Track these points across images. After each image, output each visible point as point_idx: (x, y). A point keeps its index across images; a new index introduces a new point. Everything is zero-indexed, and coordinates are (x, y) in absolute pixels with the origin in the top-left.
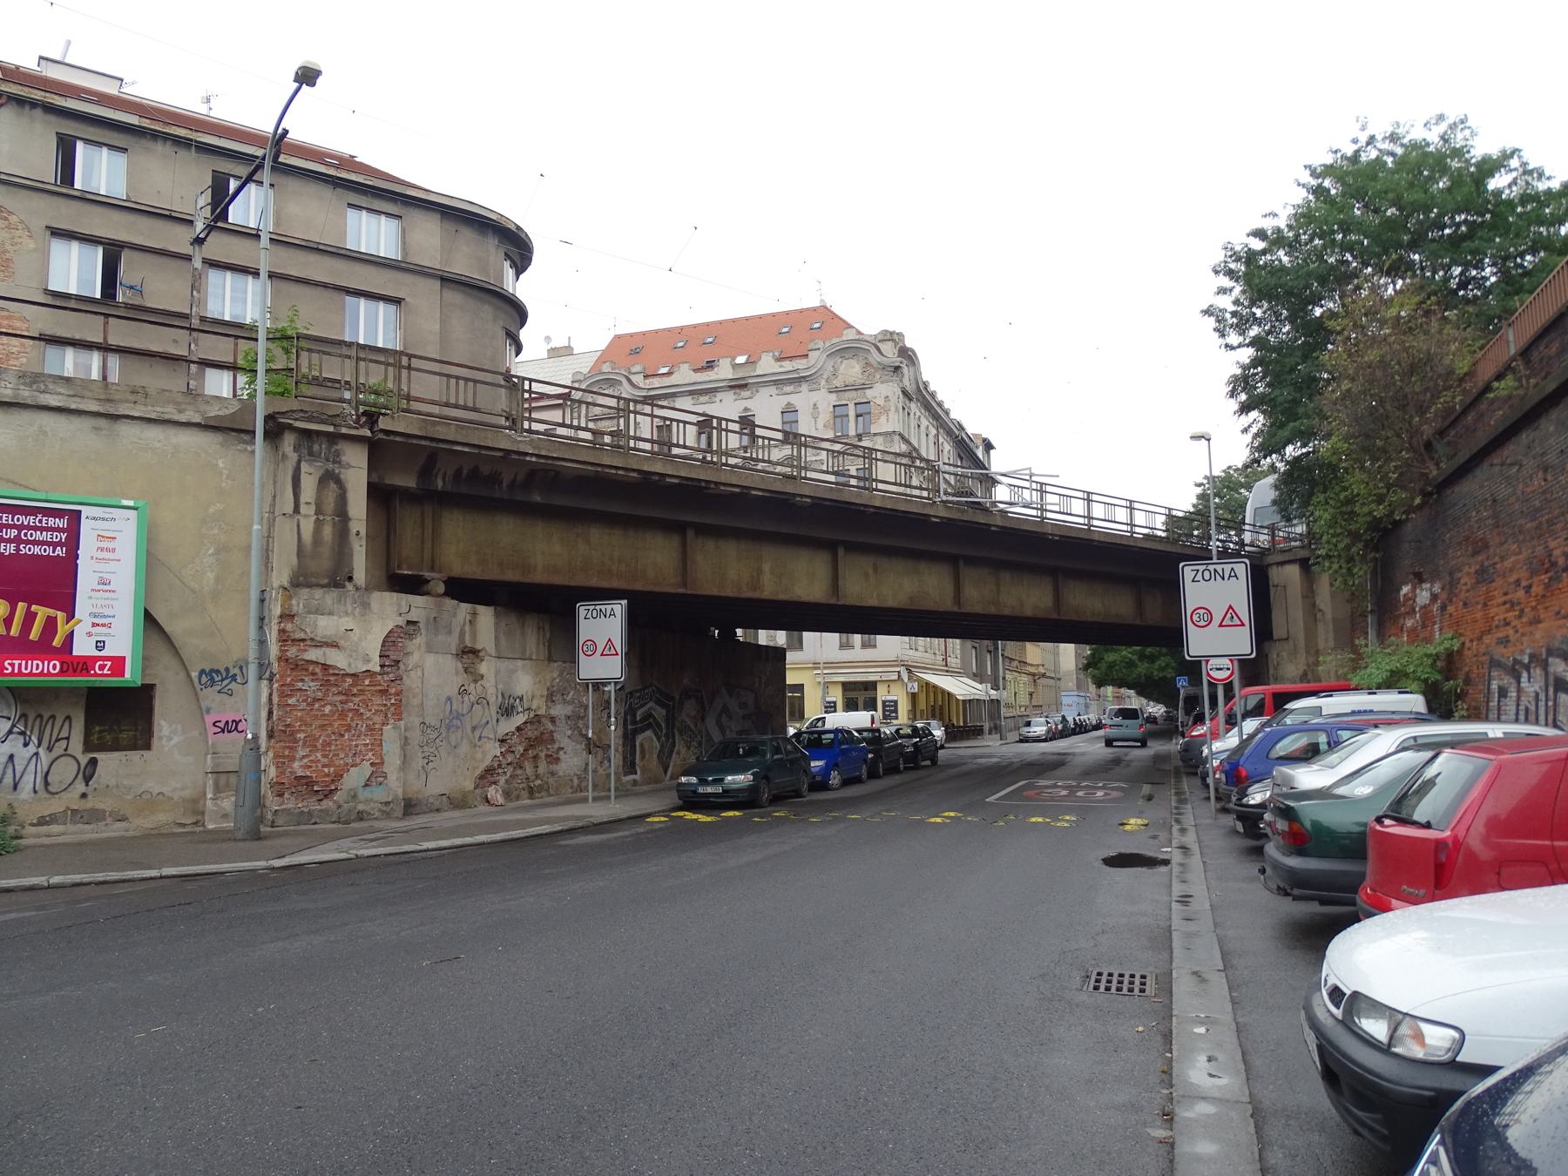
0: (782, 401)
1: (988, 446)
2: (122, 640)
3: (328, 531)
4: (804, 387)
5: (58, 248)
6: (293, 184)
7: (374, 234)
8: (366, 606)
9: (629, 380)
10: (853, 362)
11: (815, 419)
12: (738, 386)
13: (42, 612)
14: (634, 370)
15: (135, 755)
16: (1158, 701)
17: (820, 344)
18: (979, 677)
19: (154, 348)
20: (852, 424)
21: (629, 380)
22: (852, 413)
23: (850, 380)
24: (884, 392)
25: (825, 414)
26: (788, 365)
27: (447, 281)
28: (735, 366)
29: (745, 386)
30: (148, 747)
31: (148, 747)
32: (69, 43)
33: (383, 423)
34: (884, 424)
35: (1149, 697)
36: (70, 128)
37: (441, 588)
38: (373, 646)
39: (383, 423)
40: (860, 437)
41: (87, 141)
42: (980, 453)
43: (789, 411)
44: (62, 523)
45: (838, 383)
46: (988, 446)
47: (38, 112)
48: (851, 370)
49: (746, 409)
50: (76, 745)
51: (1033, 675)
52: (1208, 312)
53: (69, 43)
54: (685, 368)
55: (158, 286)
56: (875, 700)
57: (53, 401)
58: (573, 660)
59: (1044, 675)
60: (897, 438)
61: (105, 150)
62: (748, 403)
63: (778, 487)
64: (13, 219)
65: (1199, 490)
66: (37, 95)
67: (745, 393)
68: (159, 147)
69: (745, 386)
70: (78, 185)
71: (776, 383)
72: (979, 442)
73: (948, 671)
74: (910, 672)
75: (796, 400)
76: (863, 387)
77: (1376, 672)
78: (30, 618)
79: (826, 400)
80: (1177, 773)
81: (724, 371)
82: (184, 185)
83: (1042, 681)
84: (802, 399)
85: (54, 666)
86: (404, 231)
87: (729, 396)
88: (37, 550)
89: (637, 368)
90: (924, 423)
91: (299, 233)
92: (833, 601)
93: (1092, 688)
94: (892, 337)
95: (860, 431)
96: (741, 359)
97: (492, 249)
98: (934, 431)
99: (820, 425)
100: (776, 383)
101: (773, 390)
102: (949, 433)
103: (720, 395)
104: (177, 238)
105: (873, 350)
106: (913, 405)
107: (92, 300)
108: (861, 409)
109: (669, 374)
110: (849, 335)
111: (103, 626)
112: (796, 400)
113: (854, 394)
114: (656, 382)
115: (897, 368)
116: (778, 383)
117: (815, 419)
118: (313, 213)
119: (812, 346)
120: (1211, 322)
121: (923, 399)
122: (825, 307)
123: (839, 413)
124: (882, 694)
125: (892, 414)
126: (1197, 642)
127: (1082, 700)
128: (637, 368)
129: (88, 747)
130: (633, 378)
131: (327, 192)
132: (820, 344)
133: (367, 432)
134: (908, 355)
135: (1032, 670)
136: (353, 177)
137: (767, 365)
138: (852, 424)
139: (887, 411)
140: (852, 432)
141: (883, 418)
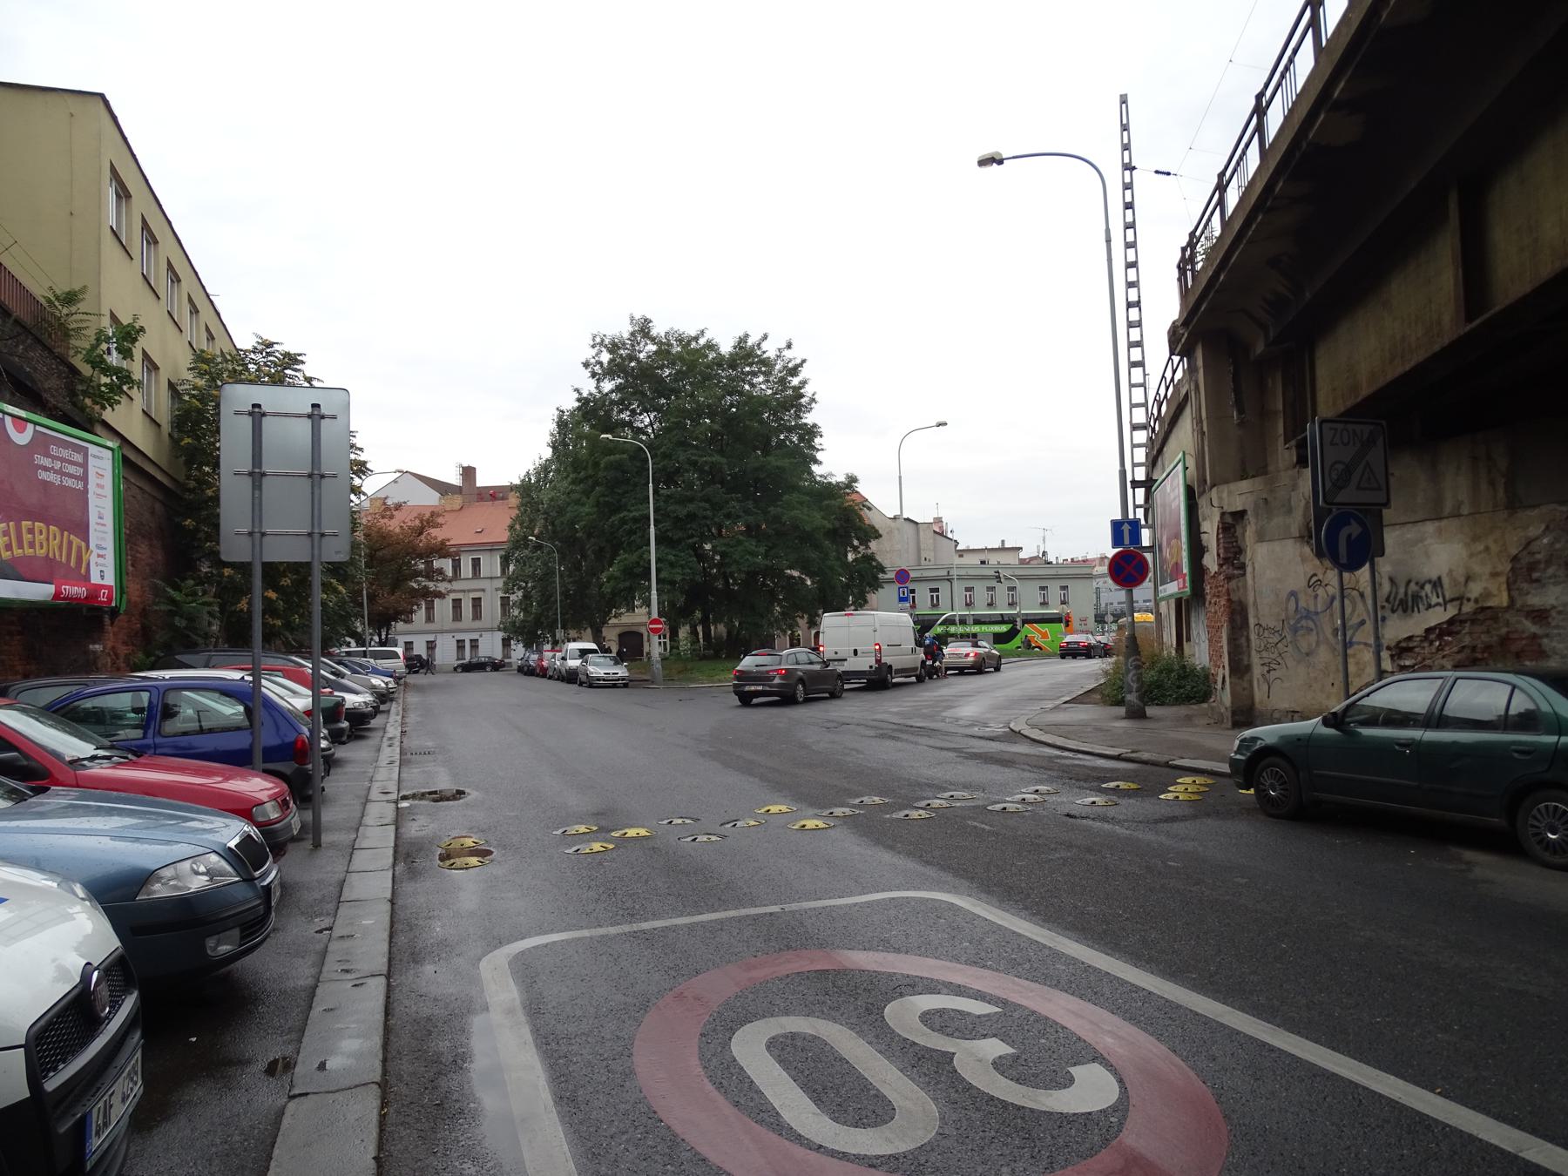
13: (76, 541)
44: (78, 458)
53: (1124, 100)
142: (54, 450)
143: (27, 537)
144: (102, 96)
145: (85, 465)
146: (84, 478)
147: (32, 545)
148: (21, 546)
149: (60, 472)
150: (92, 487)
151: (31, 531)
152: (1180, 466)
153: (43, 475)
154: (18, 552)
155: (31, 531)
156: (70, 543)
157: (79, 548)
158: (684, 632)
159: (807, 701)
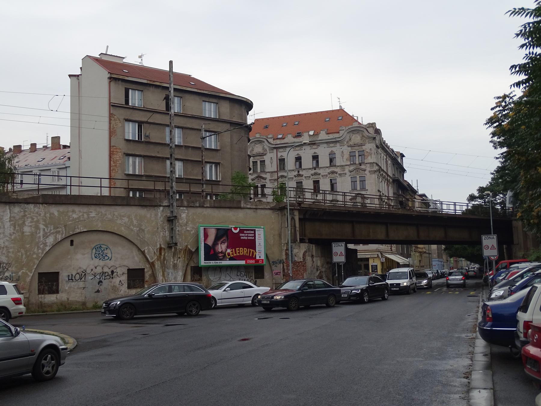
0: (329, 150)
1: (402, 156)
2: (263, 257)
3: (293, 230)
4: (338, 145)
5: (126, 124)
6: (187, 96)
7: (209, 110)
8: (300, 246)
9: (267, 141)
10: (357, 135)
11: (343, 157)
12: (312, 144)
13: (252, 250)
14: (269, 137)
15: (262, 280)
16: (475, 262)
17: (344, 128)
18: (402, 255)
19: (153, 155)
20: (357, 159)
21: (267, 141)
22: (357, 155)
23: (356, 142)
24: (369, 147)
25: (346, 156)
26: (331, 136)
27: (232, 123)
28: (310, 136)
29: (315, 144)
30: (263, 278)
31: (263, 278)
32: (108, 47)
33: (302, 205)
34: (369, 160)
35: (471, 261)
36: (128, 86)
37: (307, 241)
38: (301, 256)
39: (302, 205)
40: (360, 164)
41: (132, 89)
42: (399, 160)
43: (332, 154)
44: (253, 232)
45: (351, 143)
46: (402, 156)
47: (120, 82)
48: (356, 139)
49: (315, 153)
50: (253, 278)
51: (420, 252)
52: (491, 142)
53: (108, 47)
54: (290, 136)
55: (155, 135)
56: (368, 265)
57: (249, 206)
58: (331, 258)
59: (425, 252)
60: (375, 165)
61: (137, 91)
62: (316, 151)
63: (377, 211)
64: (115, 117)
65: (492, 176)
66: (121, 77)
67: (315, 147)
68: (152, 89)
69: (315, 144)
70: (130, 104)
71: (327, 143)
72: (399, 155)
73: (392, 253)
74: (382, 254)
75: (334, 149)
76: (361, 145)
77: (533, 257)
78: (250, 251)
79: (347, 150)
80: (483, 286)
81: (305, 139)
82: (155, 101)
83: (425, 255)
84: (337, 149)
85: (253, 261)
86: (219, 108)
87: (307, 148)
88: (250, 238)
89: (270, 136)
90: (382, 155)
91: (190, 113)
92: (387, 239)
93: (444, 257)
94: (373, 125)
95: (360, 162)
96: (311, 133)
97: (244, 111)
98: (385, 157)
99: (345, 160)
100: (327, 143)
101: (325, 145)
102: (390, 156)
103: (304, 147)
104: (158, 119)
105: (365, 131)
106: (379, 150)
107: (136, 141)
108: (361, 153)
109: (283, 138)
110: (356, 124)
111: (260, 253)
112: (334, 149)
113: (357, 148)
114: (278, 142)
115: (374, 138)
116: (328, 143)
117: (343, 157)
118: (193, 106)
119: (341, 129)
120: (492, 144)
121: (383, 147)
122: (342, 109)
123: (352, 156)
124: (371, 263)
125: (373, 156)
126: (486, 253)
127: (440, 263)
128: (270, 136)
129: (255, 278)
130: (269, 140)
131: (197, 98)
132: (344, 128)
133: (299, 208)
134: (378, 132)
135: (420, 250)
136: (202, 92)
137: (323, 136)
138: (357, 159)
139: (371, 154)
140: (357, 162)
141: (369, 158)
142: (245, 232)
143: (237, 251)
144: (102, 54)
145: (255, 234)
146: (255, 236)
147: (239, 253)
148: (236, 253)
149: (247, 236)
150: (257, 238)
151: (239, 250)
152: (385, 170)
153: (242, 238)
154: (235, 255)
155: (239, 250)
156: (250, 251)
157: (253, 252)
158: (360, 204)
159: (370, 301)
